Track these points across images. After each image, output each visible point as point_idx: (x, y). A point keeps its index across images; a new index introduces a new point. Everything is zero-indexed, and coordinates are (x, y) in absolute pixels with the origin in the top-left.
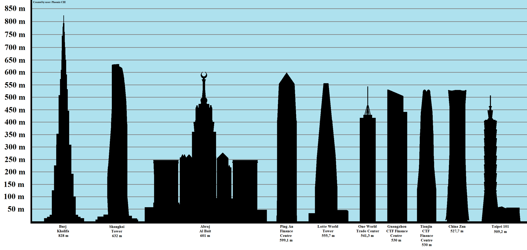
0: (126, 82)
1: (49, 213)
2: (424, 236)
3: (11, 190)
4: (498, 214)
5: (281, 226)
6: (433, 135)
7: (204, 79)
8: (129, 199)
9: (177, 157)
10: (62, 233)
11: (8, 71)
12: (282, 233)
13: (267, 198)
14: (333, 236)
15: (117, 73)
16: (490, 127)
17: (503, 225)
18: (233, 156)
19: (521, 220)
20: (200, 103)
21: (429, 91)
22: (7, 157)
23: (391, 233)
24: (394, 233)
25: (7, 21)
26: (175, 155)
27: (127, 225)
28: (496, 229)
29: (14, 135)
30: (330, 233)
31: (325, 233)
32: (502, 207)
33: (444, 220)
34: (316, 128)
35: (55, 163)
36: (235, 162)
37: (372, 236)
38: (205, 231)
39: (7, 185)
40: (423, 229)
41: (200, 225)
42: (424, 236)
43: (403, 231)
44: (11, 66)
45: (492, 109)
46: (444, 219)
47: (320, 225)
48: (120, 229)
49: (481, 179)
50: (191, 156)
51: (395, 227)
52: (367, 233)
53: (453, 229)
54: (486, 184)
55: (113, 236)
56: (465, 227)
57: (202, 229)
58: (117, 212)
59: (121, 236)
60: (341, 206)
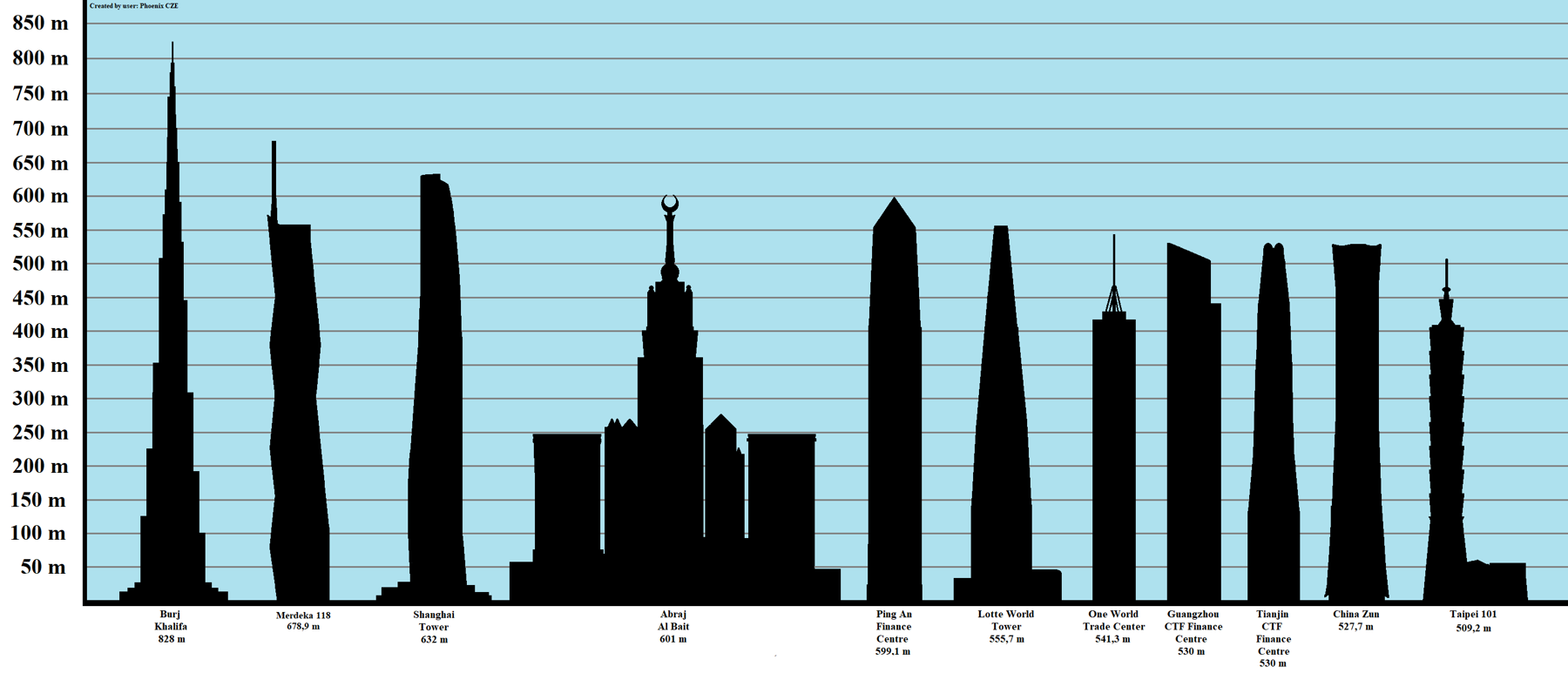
0: (459, 223)
1: (133, 577)
2: (1267, 640)
3: (29, 516)
4: (1462, 580)
6: (1289, 365)
8: (468, 541)
9: (598, 426)
10: (169, 633)
11: (22, 192)
12: (881, 632)
13: (841, 534)
14: (1020, 640)
15: (435, 195)
16: (1447, 344)
17: (1480, 609)
18: (749, 422)
19: (1530, 597)
20: (660, 279)
21: (1280, 246)
22: (19, 427)
23: (1178, 632)
25: (18, 57)
27: (459, 610)
28: (1462, 621)
29: (38, 365)
30: (1011, 631)
31: (999, 632)
32: (1478, 562)
33: (1321, 597)
34: (973, 348)
36: (753, 439)
37: (1126, 640)
38: (674, 626)
39: (20, 501)
41: (660, 609)
42: (1267, 640)
43: (1210, 627)
45: (1451, 294)
46: (1321, 595)
47: (986, 609)
48: (443, 622)
50: (636, 422)
51: (1189, 615)
52: (1112, 633)
53: (1345, 620)
54: (1434, 499)
55: (423, 640)
56: (1377, 615)
57: (664, 621)
58: (435, 574)
59: (444, 640)
60: (1042, 557)
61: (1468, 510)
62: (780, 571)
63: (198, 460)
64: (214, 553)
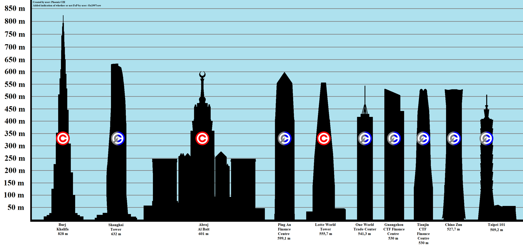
0: (125, 82)
1: (49, 211)
2: (421, 234)
3: (11, 189)
4: (494, 213)
5: (279, 224)
7: (202, 78)
8: (128, 198)
9: (176, 156)
10: (62, 231)
11: (8, 70)
12: (280, 231)
13: (265, 196)
14: (331, 234)
15: (116, 72)
17: (499, 223)
18: (231, 155)
19: (517, 219)
20: (199, 102)
21: (426, 90)
22: (7, 156)
23: (388, 231)
24: (391, 231)
25: (7, 21)
26: (174, 154)
27: (126, 223)
28: (492, 227)
29: (14, 133)
30: (327, 231)
31: (323, 231)
32: (498, 205)
33: (441, 218)
35: (54, 162)
36: (233, 161)
37: (369, 234)
38: (204, 229)
39: (7, 183)
40: (420, 227)
41: (199, 223)
42: (421, 234)
43: (400, 230)
44: (11, 65)
45: (488, 108)
46: (441, 218)
47: (318, 223)
48: (119, 227)
49: (478, 177)
50: (190, 155)
51: (392, 225)
52: (364, 231)
53: (449, 227)
54: (482, 182)
55: (112, 234)
56: (461, 225)
57: (200, 227)
58: (116, 210)
59: (120, 234)
60: (338, 204)
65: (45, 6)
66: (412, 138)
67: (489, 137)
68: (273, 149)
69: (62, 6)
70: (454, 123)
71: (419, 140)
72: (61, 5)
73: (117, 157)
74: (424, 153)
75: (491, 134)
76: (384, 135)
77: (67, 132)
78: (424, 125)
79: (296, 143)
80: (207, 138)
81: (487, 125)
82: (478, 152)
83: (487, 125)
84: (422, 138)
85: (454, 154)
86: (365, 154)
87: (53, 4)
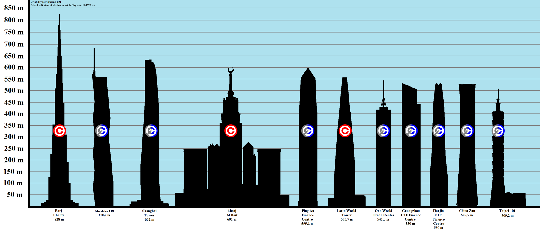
0: (158, 76)
1: (46, 198)
2: (436, 220)
3: (10, 177)
4: (504, 199)
8: (161, 186)
9: (206, 146)
10: (58, 217)
11: (7, 66)
12: (304, 217)
13: (290, 183)
14: (351, 220)
15: (150, 67)
17: (510, 209)
18: (258, 145)
19: (527, 205)
20: (227, 96)
21: (441, 85)
22: (6, 147)
23: (406, 217)
25: (6, 20)
27: (158, 209)
28: (504, 213)
29: (13, 125)
30: (348, 217)
31: (344, 217)
32: (509, 193)
33: (455, 205)
36: (259, 151)
37: (388, 220)
38: (232, 215)
39: (7, 172)
41: (227, 209)
42: (436, 220)
43: (417, 215)
45: (500, 101)
46: (455, 204)
47: (339, 209)
48: (153, 213)
49: (490, 166)
50: (219, 145)
51: (410, 211)
52: (383, 217)
53: (463, 213)
54: (494, 171)
55: (146, 220)
56: (474, 211)
57: (229, 213)
58: (150, 197)
59: (153, 220)
60: (359, 191)
61: (505, 175)
62: (269, 196)
63: (68, 158)
64: (74, 190)
65: (42, 5)
66: (427, 131)
67: (500, 129)
68: (298, 139)
69: (58, 5)
70: (468, 116)
71: (435, 132)
72: (57, 5)
73: (150, 149)
74: (439, 144)
75: (503, 126)
76: (401, 127)
77: (63, 124)
78: (439, 118)
79: (319, 134)
80: (235, 131)
81: (498, 118)
82: (490, 143)
83: (498, 118)
84: (438, 130)
85: (468, 146)
86: (383, 145)
87: (50, 4)
